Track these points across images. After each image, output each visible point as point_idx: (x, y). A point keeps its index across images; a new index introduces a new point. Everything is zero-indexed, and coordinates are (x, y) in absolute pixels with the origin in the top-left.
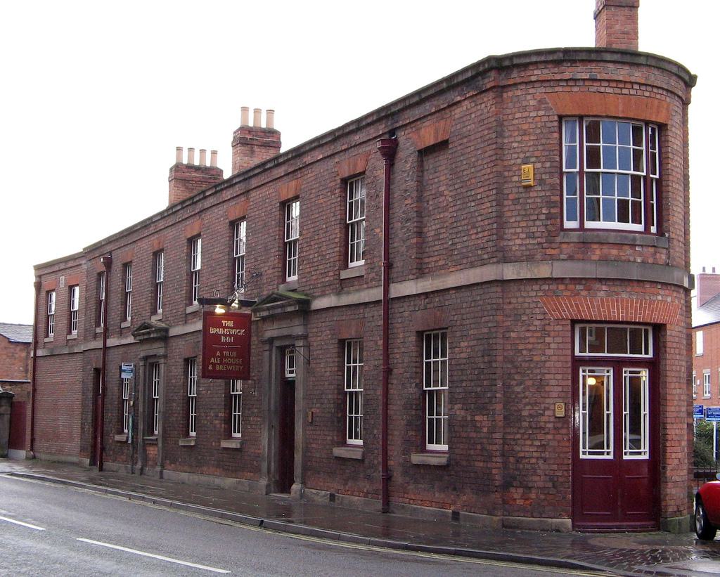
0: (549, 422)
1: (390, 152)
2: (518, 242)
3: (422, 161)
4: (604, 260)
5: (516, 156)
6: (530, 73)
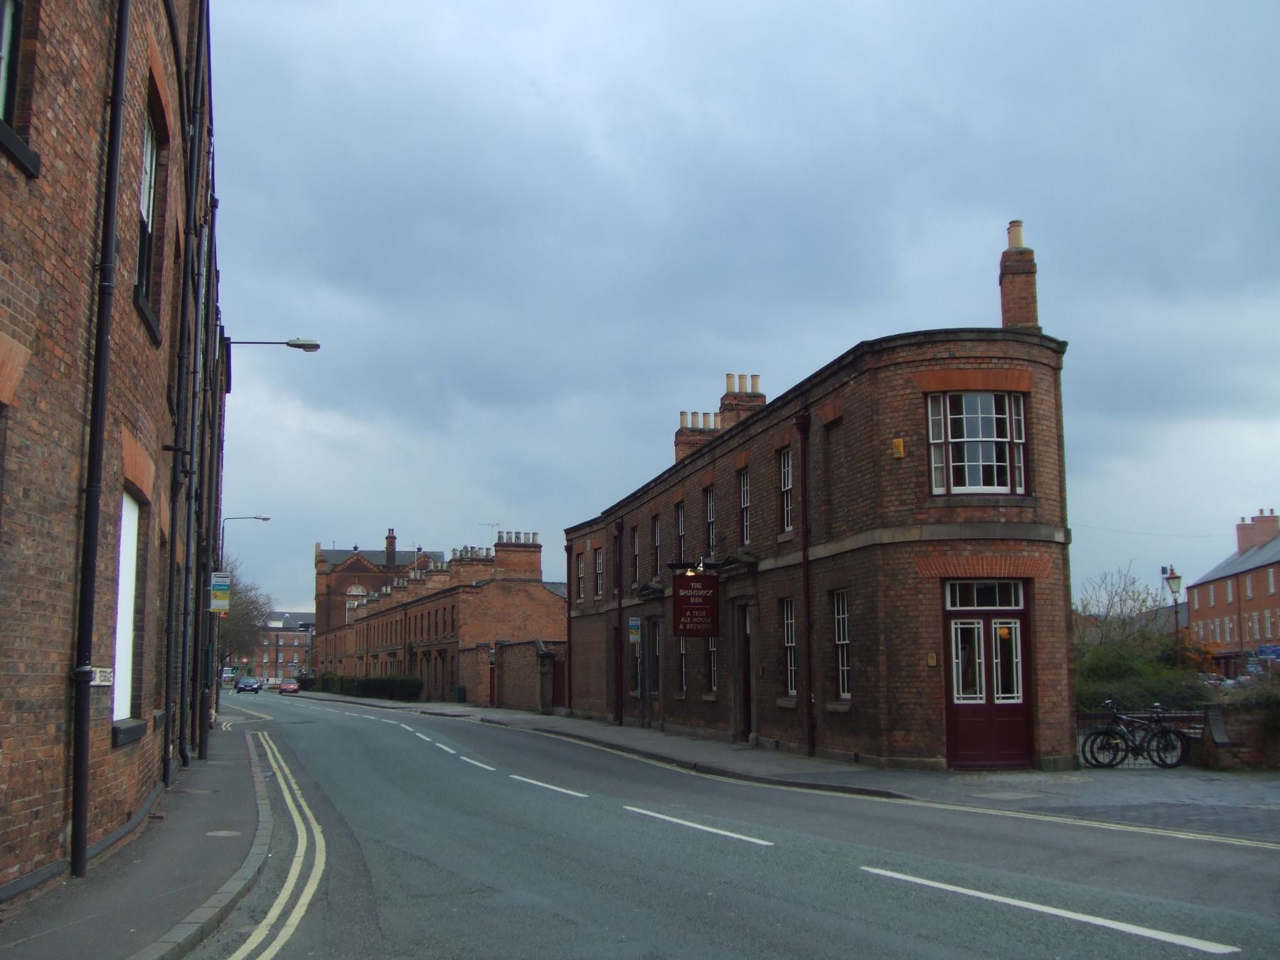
0: (924, 671)
1: (804, 426)
2: (893, 508)
3: (828, 435)
4: (969, 522)
5: (888, 431)
6: (896, 355)
